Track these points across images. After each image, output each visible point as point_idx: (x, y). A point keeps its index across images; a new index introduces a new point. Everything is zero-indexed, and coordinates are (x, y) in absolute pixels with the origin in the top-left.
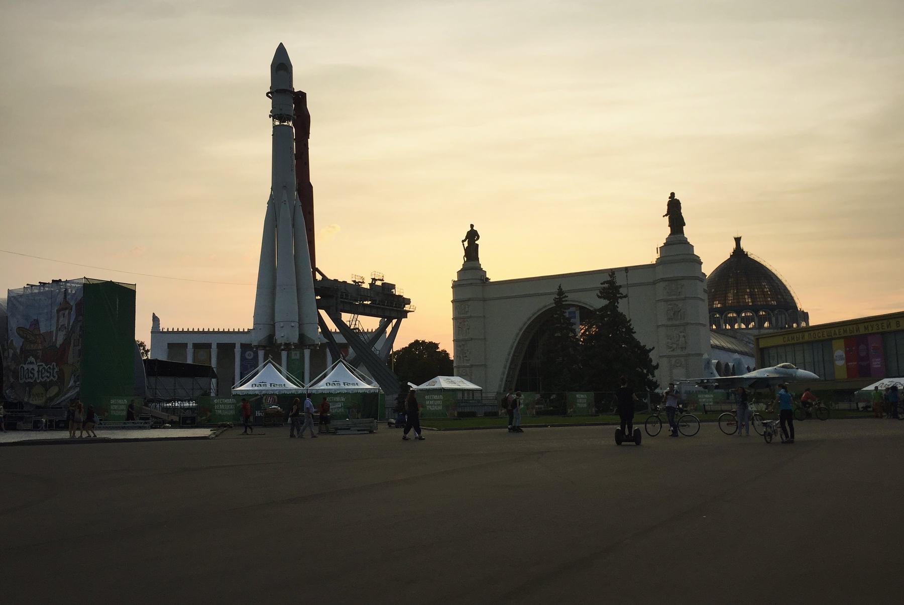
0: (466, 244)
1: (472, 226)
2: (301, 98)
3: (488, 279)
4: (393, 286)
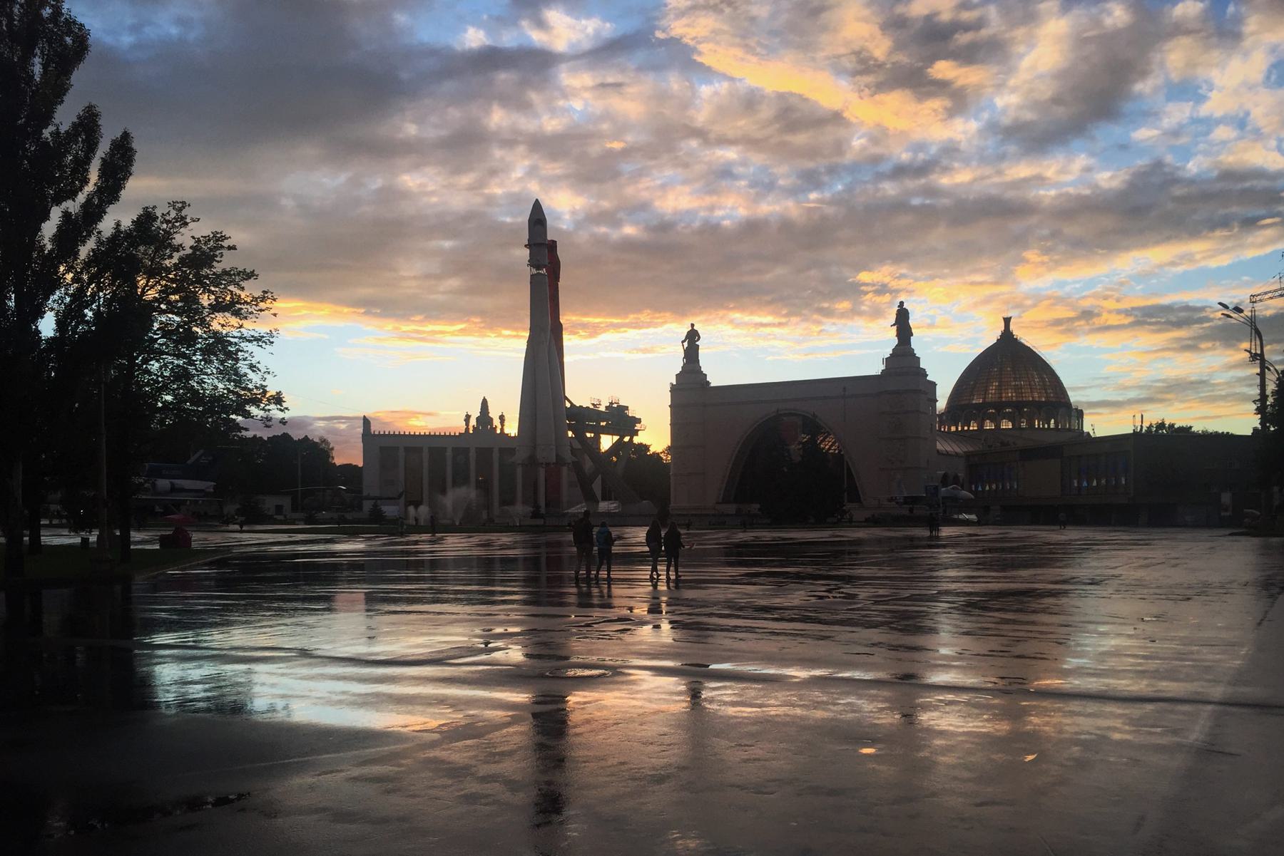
0: (686, 344)
2: (553, 246)
3: (708, 383)
4: (627, 408)
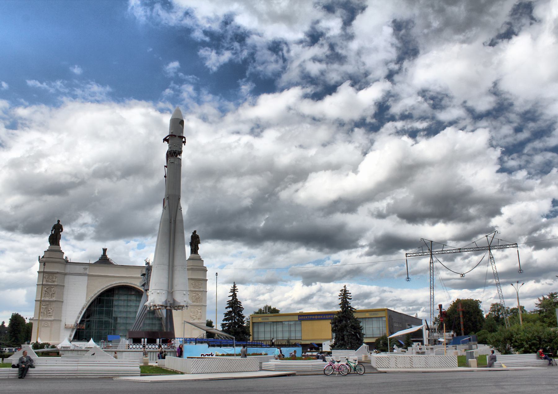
1: (59, 221)
